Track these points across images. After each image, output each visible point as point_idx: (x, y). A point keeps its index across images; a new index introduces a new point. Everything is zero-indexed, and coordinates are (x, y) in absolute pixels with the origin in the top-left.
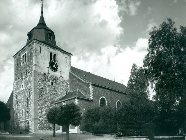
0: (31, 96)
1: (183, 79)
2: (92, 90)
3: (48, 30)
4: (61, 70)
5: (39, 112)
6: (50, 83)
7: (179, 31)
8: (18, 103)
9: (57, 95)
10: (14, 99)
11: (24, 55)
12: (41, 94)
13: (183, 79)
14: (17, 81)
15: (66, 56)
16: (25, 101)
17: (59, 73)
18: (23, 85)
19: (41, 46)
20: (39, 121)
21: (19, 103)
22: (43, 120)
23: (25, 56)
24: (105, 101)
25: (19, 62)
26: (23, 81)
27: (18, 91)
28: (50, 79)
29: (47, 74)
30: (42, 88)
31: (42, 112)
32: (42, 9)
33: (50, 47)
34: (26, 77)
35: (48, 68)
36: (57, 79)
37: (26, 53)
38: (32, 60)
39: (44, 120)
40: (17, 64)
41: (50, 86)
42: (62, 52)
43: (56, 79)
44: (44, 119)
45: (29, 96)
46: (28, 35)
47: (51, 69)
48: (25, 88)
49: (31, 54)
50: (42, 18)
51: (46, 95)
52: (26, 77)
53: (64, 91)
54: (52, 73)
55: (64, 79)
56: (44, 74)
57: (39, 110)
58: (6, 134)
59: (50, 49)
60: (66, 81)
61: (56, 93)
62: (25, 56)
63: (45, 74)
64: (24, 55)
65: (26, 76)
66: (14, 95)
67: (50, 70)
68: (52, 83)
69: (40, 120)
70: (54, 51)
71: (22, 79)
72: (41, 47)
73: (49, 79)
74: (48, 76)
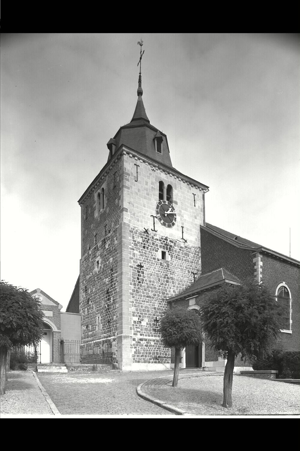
0: (115, 284)
1: (201, 312)
4: (183, 224)
5: (135, 322)
6: (159, 255)
8: (90, 303)
9: (173, 283)
10: (81, 295)
12: (138, 279)
13: (201, 312)
14: (86, 255)
15: (194, 190)
16: (104, 297)
17: (178, 230)
18: (98, 262)
19: (138, 162)
20: (134, 342)
21: (91, 302)
22: (141, 340)
26: (98, 253)
27: (88, 277)
29: (150, 232)
30: (141, 266)
31: (140, 322)
32: (140, 85)
33: (159, 169)
34: (104, 242)
35: (154, 217)
36: (175, 244)
37: (104, 186)
38: (117, 200)
39: (146, 340)
40: (87, 218)
41: (159, 260)
42: (186, 182)
43: (172, 244)
44: (145, 337)
45: (112, 286)
46: (109, 146)
47: (160, 220)
48: (102, 267)
49: (115, 187)
50: (140, 106)
51: (150, 282)
52: (105, 243)
54: (162, 231)
55: (189, 244)
56: (144, 232)
57: (134, 315)
58: (61, 371)
59: (159, 171)
60: (193, 249)
61: (172, 278)
62: (101, 195)
63: (146, 231)
65: (105, 240)
66: (82, 286)
67: (159, 226)
68: (164, 254)
69: (137, 340)
70: (167, 179)
71: (97, 249)
72: (137, 166)
73: (157, 245)
74: (153, 238)
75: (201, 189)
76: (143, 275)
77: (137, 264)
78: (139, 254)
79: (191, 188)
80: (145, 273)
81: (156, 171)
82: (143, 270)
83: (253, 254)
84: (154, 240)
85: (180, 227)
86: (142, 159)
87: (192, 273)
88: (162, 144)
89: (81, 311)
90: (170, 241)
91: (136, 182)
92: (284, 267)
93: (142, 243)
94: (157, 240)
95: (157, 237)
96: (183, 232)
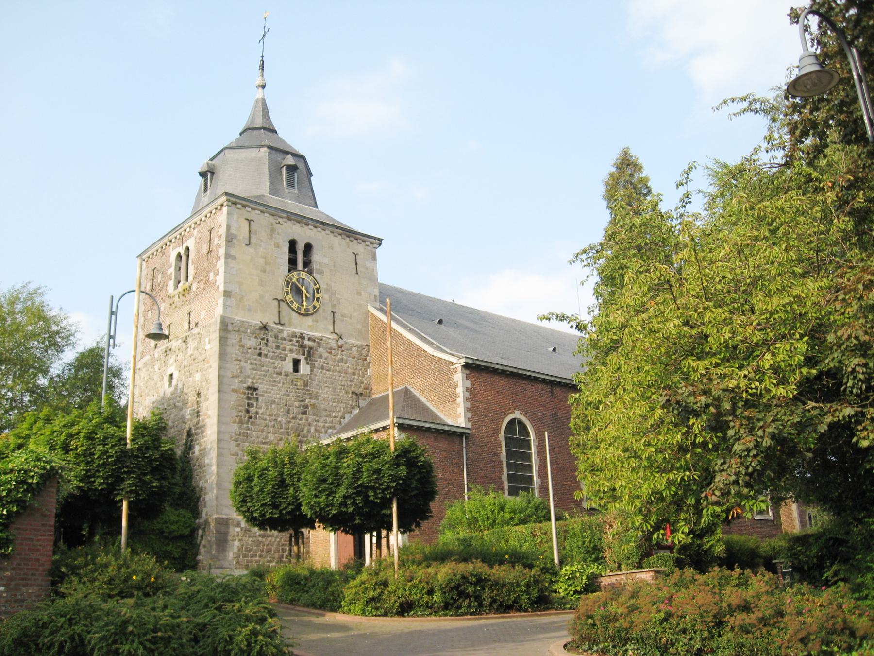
2: (467, 389)
3: (279, 151)
6: (289, 367)
7: (725, 555)
11: (182, 253)
18: (171, 375)
23: (184, 258)
24: (528, 434)
25: (159, 279)
28: (288, 345)
35: (279, 301)
36: (319, 343)
38: (212, 274)
41: (287, 375)
49: (210, 251)
53: (347, 393)
61: (314, 406)
62: (184, 258)
64: (182, 253)
68: (296, 363)
75: (367, 243)
76: (257, 405)
77: (245, 385)
78: (250, 367)
79: (351, 243)
80: (260, 400)
81: (284, 224)
82: (257, 394)
83: (453, 367)
84: (279, 341)
85: (329, 312)
86: (258, 210)
87: (353, 393)
88: (296, 174)
89: (222, 541)
90: (309, 339)
91: (247, 247)
92: (515, 385)
93: (255, 349)
94: (285, 339)
95: (285, 335)
96: (334, 322)
